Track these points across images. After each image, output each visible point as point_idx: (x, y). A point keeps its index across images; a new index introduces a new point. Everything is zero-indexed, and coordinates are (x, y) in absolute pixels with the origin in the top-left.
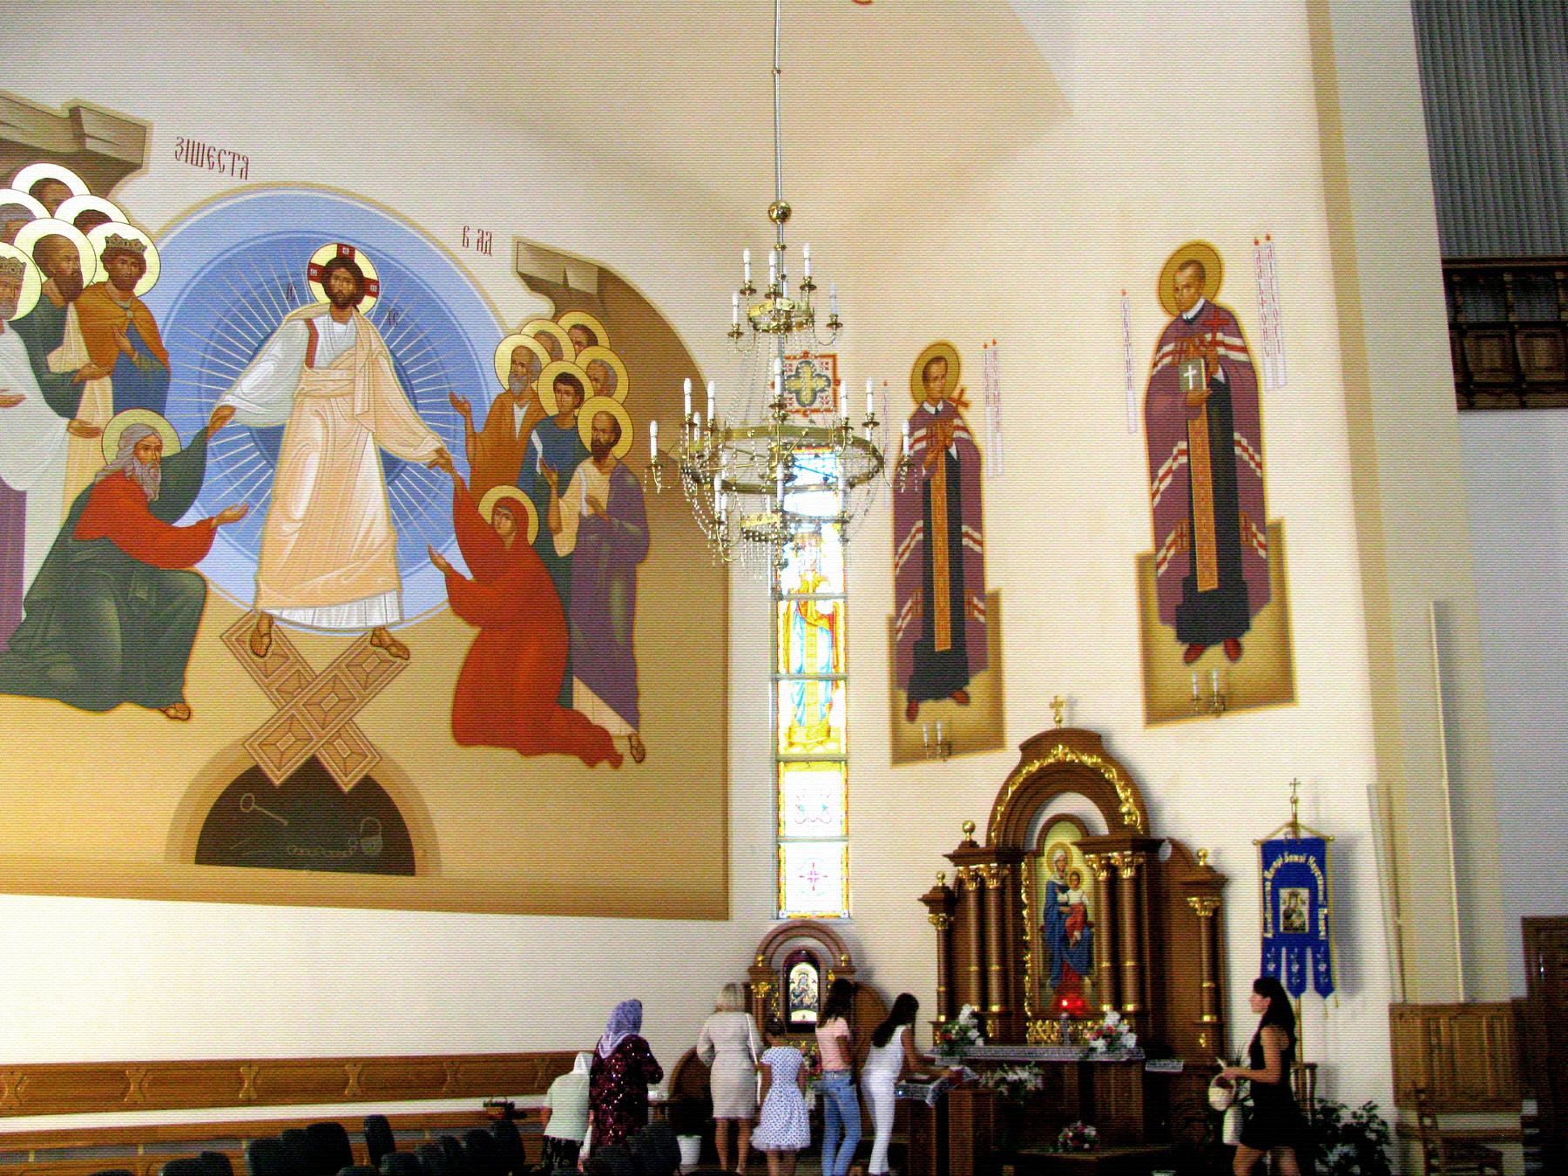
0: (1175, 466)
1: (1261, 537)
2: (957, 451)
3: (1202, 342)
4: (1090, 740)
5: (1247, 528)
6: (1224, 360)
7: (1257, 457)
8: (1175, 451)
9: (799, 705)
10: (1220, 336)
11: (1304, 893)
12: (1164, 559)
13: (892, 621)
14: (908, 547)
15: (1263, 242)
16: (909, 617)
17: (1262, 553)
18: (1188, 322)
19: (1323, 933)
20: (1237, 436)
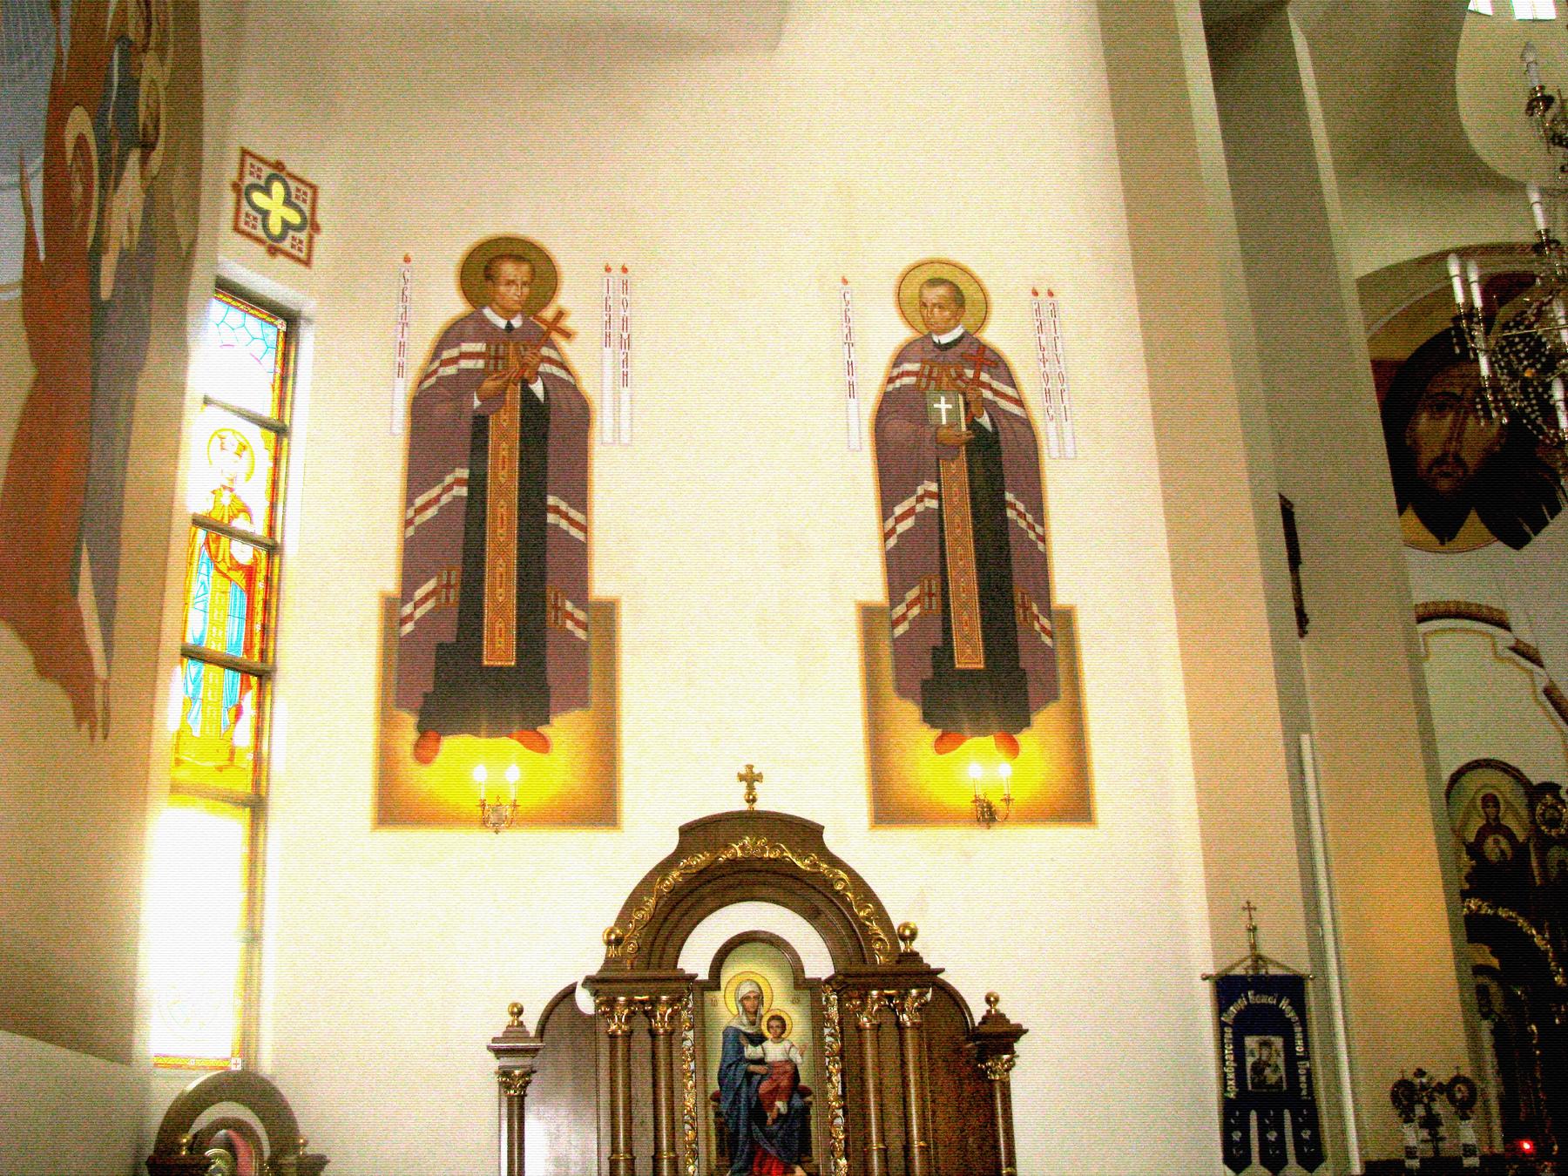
0: (919, 508)
1: (1045, 622)
2: (545, 388)
3: (960, 376)
4: (808, 834)
5: (1026, 608)
6: (991, 407)
7: (1039, 529)
8: (920, 490)
9: (194, 698)
10: (984, 377)
11: (1278, 1042)
12: (904, 617)
13: (391, 608)
14: (437, 499)
15: (1043, 295)
16: (430, 604)
17: (1047, 640)
18: (939, 346)
19: (1304, 1092)
20: (1009, 497)
